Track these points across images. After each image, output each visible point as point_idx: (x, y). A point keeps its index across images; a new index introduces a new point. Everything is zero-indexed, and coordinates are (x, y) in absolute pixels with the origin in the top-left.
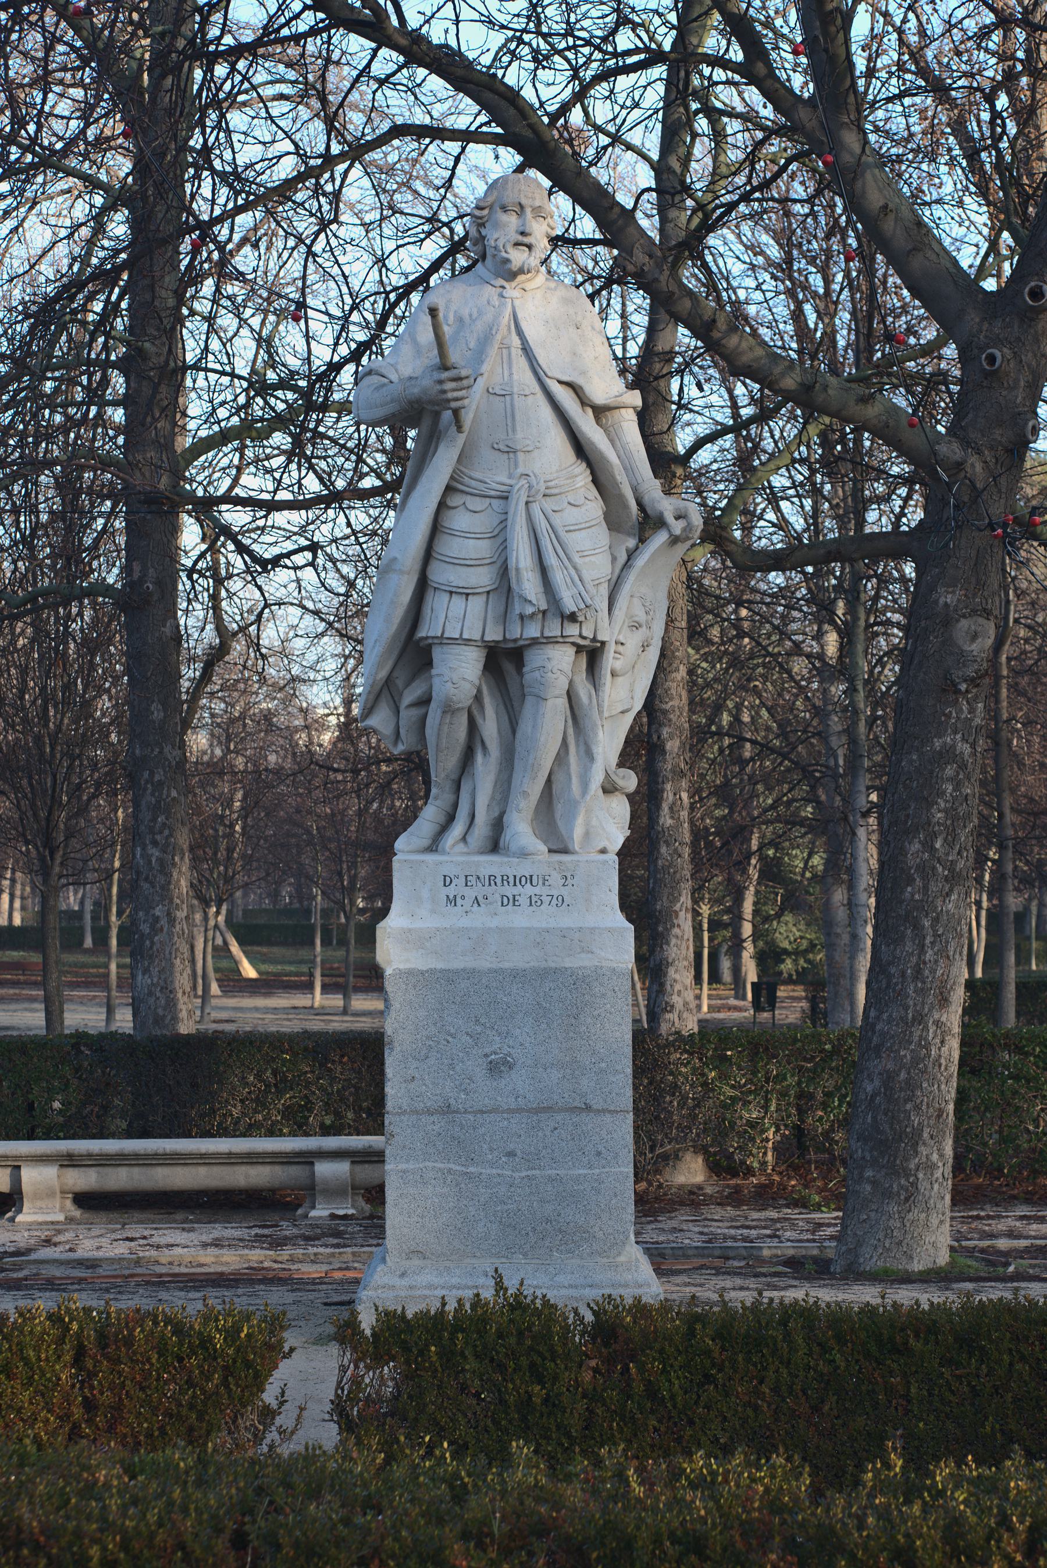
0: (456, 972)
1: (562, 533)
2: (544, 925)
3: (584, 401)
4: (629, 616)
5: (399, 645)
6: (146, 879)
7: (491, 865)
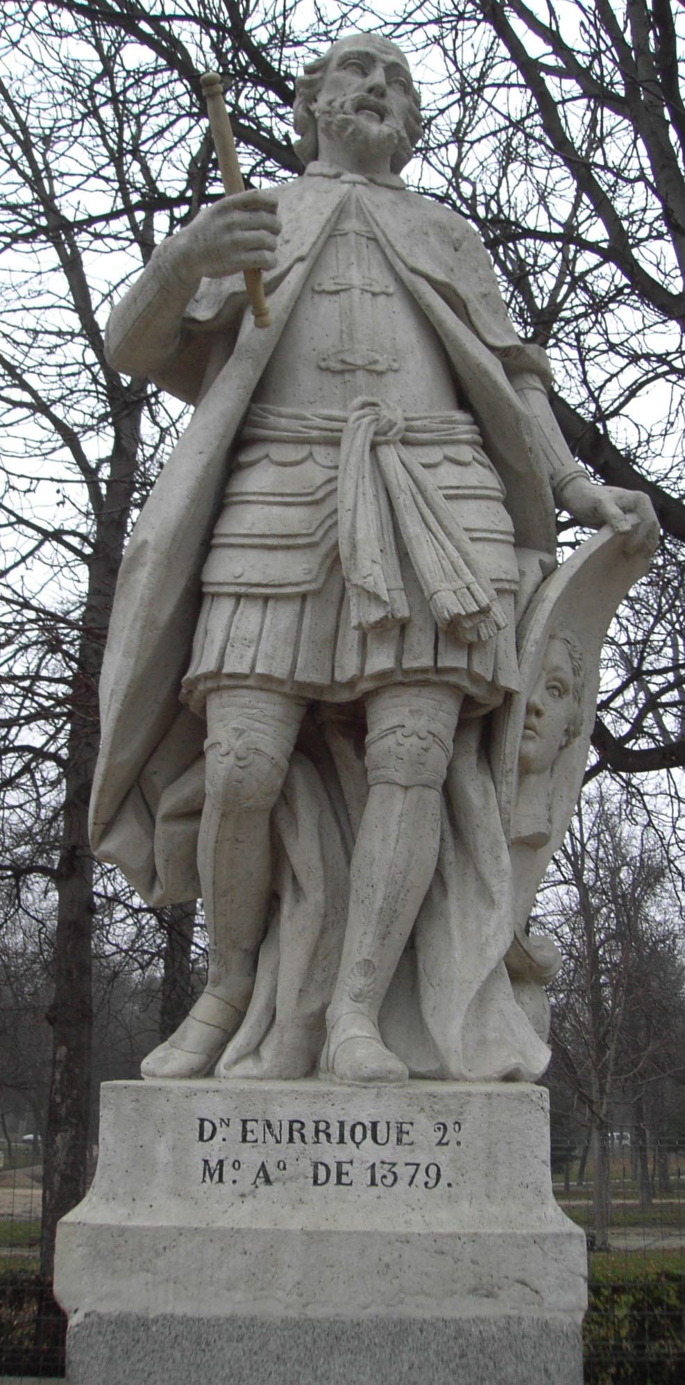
0: (214, 1324)
2: (401, 1229)
7: (292, 1101)
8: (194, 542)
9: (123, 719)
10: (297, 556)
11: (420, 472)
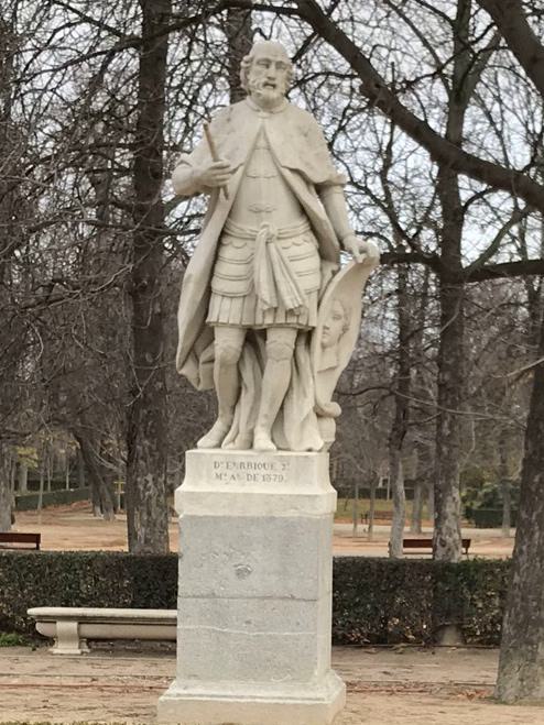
0: (219, 517)
1: (287, 262)
3: (307, 182)
4: (333, 311)
5: (196, 330)
6: (142, 458)
8: (209, 272)
9: (187, 332)
10: (239, 283)
11: (281, 250)
